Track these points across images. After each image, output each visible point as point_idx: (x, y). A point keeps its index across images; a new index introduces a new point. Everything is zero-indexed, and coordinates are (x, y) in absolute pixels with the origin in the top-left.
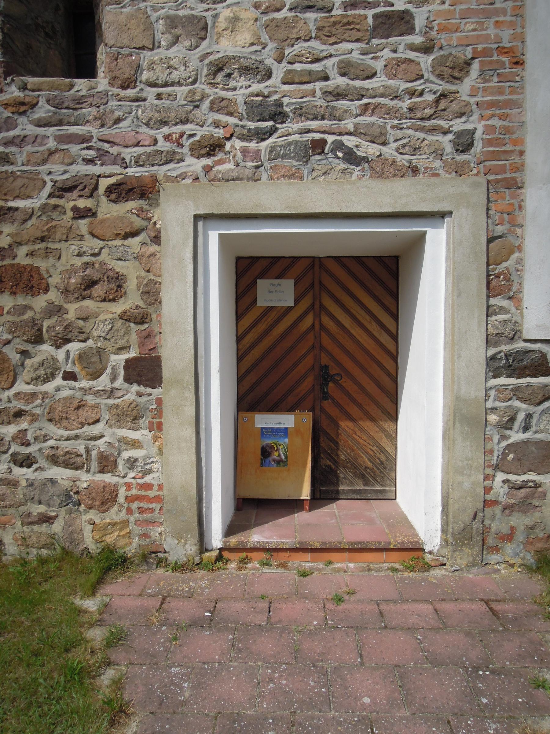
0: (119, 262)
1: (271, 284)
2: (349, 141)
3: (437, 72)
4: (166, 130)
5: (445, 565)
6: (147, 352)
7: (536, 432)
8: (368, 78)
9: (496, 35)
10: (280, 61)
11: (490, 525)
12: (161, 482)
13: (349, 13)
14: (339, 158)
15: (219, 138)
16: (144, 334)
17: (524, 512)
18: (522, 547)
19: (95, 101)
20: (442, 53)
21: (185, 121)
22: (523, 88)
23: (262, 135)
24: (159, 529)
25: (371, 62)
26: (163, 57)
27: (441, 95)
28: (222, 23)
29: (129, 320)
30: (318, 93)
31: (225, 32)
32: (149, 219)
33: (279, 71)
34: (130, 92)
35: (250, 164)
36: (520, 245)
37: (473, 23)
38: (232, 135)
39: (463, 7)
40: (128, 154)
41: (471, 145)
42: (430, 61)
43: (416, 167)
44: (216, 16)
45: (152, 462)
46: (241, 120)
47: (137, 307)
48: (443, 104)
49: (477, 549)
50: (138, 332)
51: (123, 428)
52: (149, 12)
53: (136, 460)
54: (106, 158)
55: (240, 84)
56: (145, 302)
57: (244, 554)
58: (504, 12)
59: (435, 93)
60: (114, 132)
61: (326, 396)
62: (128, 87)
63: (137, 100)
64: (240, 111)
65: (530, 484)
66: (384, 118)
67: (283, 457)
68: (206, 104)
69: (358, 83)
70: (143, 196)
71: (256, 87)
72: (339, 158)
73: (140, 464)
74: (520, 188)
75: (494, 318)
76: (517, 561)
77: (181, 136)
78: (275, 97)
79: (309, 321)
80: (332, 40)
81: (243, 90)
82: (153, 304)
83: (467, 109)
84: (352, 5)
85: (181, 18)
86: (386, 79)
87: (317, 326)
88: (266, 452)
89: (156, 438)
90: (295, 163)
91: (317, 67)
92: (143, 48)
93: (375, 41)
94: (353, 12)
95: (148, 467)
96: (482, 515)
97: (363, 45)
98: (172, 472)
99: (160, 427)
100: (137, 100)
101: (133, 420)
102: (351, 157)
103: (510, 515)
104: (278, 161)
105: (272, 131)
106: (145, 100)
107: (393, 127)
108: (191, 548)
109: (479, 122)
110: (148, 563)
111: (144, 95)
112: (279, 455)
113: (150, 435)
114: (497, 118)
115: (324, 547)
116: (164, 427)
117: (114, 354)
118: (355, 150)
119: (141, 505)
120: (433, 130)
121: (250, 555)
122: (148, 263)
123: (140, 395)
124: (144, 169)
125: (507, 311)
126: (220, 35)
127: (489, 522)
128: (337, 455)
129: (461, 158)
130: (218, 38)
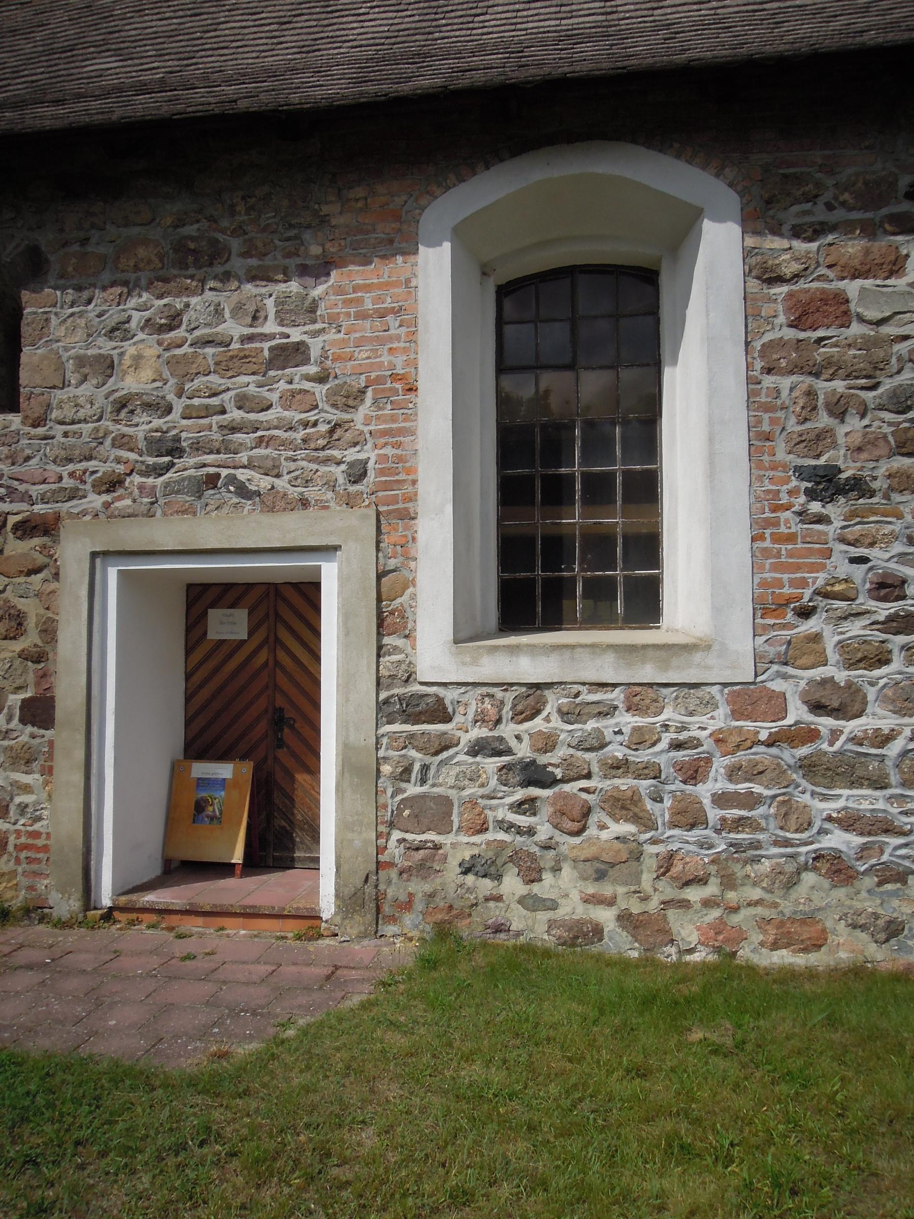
0: (22, 599)
1: (223, 615)
2: (242, 475)
3: (330, 402)
4: (71, 467)
5: (337, 935)
6: (42, 692)
7: (433, 785)
8: (263, 410)
9: (390, 362)
10: (180, 397)
11: (386, 891)
12: (50, 830)
13: (246, 346)
14: (231, 492)
15: (120, 474)
16: (41, 673)
17: (424, 878)
18: (421, 917)
20: (337, 382)
21: (89, 458)
22: (416, 415)
23: (159, 470)
24: (46, 882)
25: (267, 395)
26: (71, 395)
27: (336, 425)
28: (127, 360)
29: (26, 659)
30: (215, 428)
31: (130, 369)
32: (51, 556)
33: (179, 406)
34: (41, 431)
35: (146, 500)
36: (413, 580)
37: (367, 351)
38: (132, 471)
39: (357, 335)
40: (35, 491)
41: (365, 474)
42: (324, 392)
43: (307, 500)
44: (122, 354)
45: (42, 809)
46: (141, 456)
47: (36, 645)
49: (370, 917)
50: (36, 671)
51: (17, 771)
52: (61, 353)
53: (27, 806)
54: (14, 495)
55: (142, 420)
56: (42, 640)
57: (134, 916)
58: (398, 338)
59: (329, 423)
60: (23, 470)
61: (280, 744)
62: (38, 426)
63: (45, 438)
64: (140, 447)
65: (429, 844)
66: (280, 450)
67: (218, 813)
68: (108, 442)
69: (252, 416)
70: (46, 533)
71: (157, 423)
72: (231, 492)
73: (30, 810)
74: (413, 519)
75: (387, 658)
76: (415, 933)
77: (84, 473)
78: (174, 432)
79: (263, 656)
80: (230, 374)
81: (144, 425)
82: (50, 642)
83: (361, 439)
84: (249, 338)
85: (89, 357)
86: (281, 410)
87: (271, 663)
88: (200, 807)
89: (46, 783)
90: (188, 499)
91: (215, 401)
92: (54, 387)
93: (272, 373)
94: (250, 346)
95: (38, 813)
96: (375, 878)
97: (259, 378)
98: (60, 820)
99: (51, 769)
100: (45, 438)
101: (27, 763)
102: (243, 491)
103: (408, 880)
104: (170, 498)
105: (170, 466)
106: (53, 438)
107: (286, 459)
108: (75, 904)
109: (373, 451)
110: (30, 918)
111: (51, 433)
112: (214, 810)
113: (41, 779)
114: (389, 447)
115: (214, 910)
116: (54, 772)
117: (12, 693)
118: (247, 484)
119: (29, 854)
120: (327, 461)
121: (141, 916)
122: (47, 599)
123: (33, 737)
124: (49, 506)
125: (401, 651)
126: (125, 373)
127: (385, 887)
128: (293, 814)
129: (353, 489)
130: (124, 376)
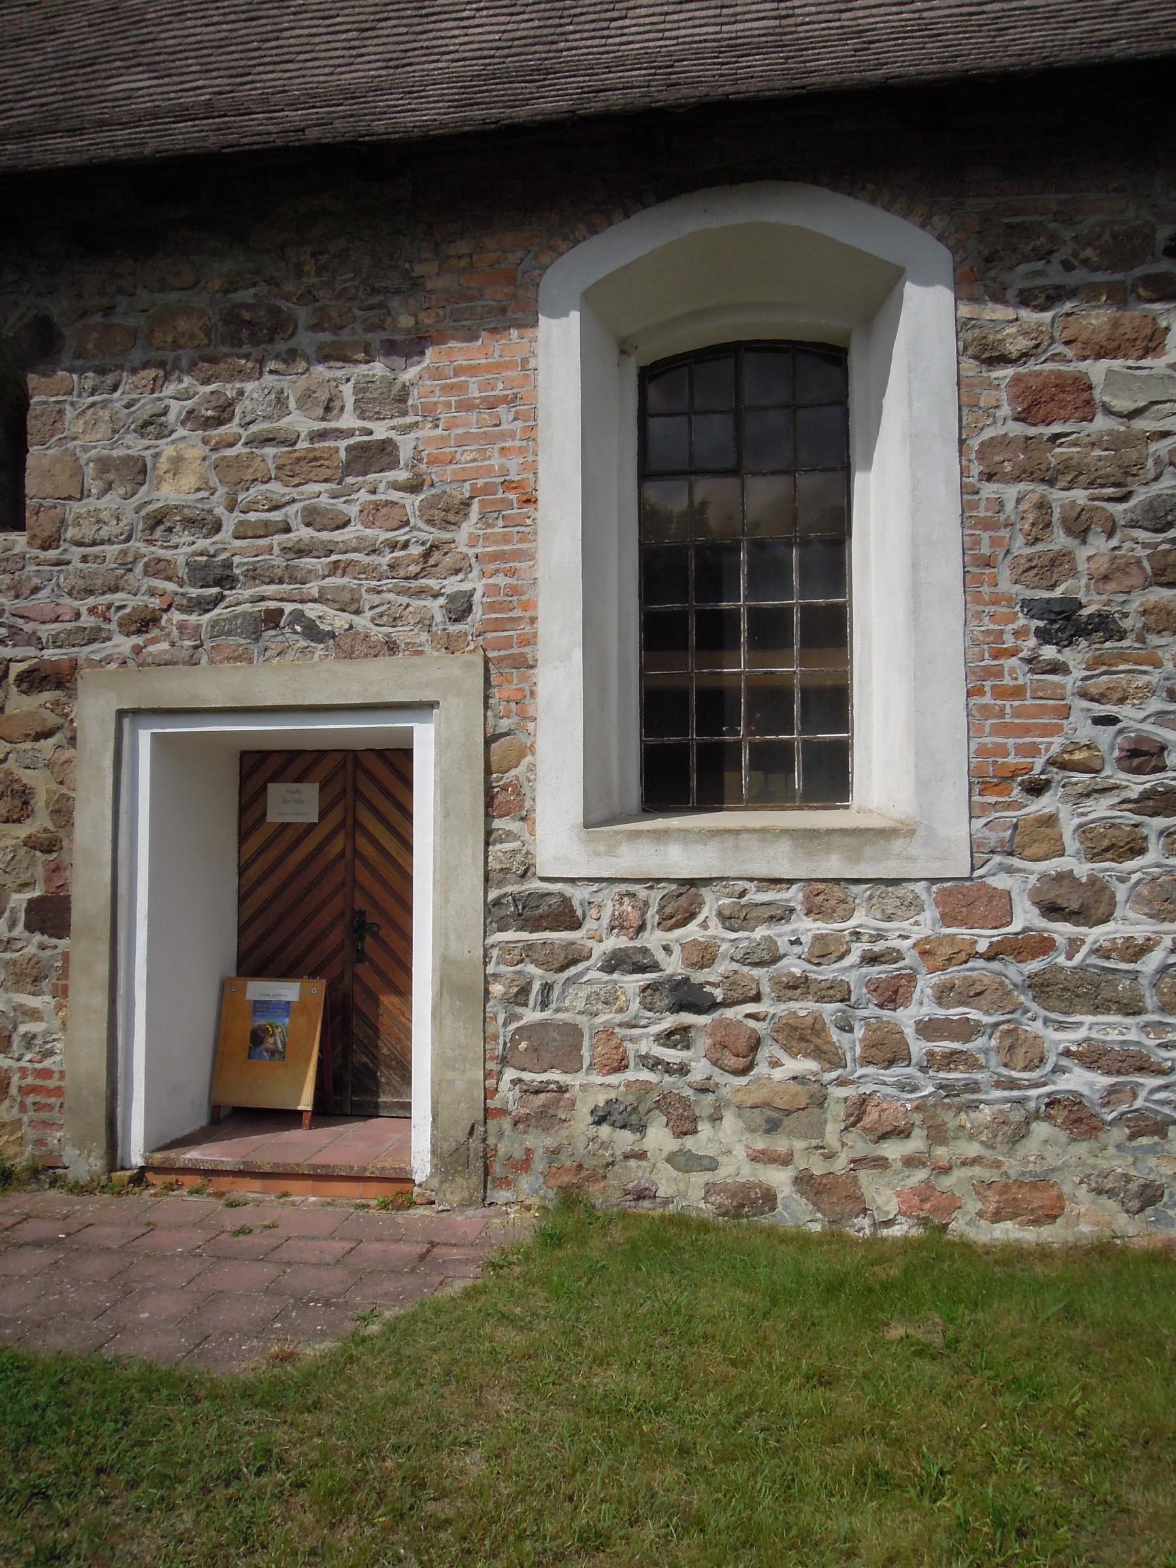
0: (28, 771)
1: (287, 791)
2: (312, 611)
3: (425, 518)
4: (91, 601)
5: (433, 1203)
6: (54, 890)
7: (558, 1010)
8: (338, 528)
9: (502, 466)
10: (231, 510)
11: (496, 1146)
12: (64, 1067)
13: (316, 445)
14: (297, 633)
15: (154, 610)
16: (52, 866)
17: (546, 1130)
18: (541, 1180)
19: (10, 566)
20: (433, 491)
21: (115, 589)
22: (535, 533)
23: (204, 605)
24: (59, 1134)
25: (344, 508)
27: (432, 546)
28: (163, 464)
29: (34, 848)
30: (276, 550)
31: (168, 475)
32: (66, 715)
33: (230, 522)
34: (52, 554)
35: (188, 643)
36: (532, 745)
37: (472, 451)
38: (170, 606)
39: (460, 431)
40: (46, 631)
41: (469, 609)
42: (417, 504)
43: (395, 643)
44: (157, 456)
45: (54, 1040)
46: (181, 586)
47: (46, 830)
48: (435, 557)
49: (476, 1180)
50: (46, 863)
51: (22, 992)
52: (78, 454)
53: (34, 1037)
54: (18, 637)
55: (182, 540)
56: (55, 824)
57: (172, 1178)
58: (512, 435)
59: (423, 544)
60: (30, 604)
62: (49, 547)
63: (58, 563)
64: (180, 575)
65: (552, 1086)
66: (360, 579)
67: (280, 1046)
68: (139, 568)
69: (325, 535)
70: (59, 685)
71: (202, 544)
72: (297, 633)
73: (38, 1041)
74: (532, 667)
75: (498, 847)
76: (534, 1201)
77: (109, 608)
78: (223, 556)
79: (338, 844)
80: (296, 481)
81: (186, 547)
82: (64, 826)
83: (465, 564)
84: (320, 435)
85: (115, 460)
86: (362, 528)
87: (349, 853)
88: (257, 1037)
89: (60, 1007)
90: (242, 641)
91: (276, 516)
92: (69, 498)
93: (350, 480)
94: (321, 445)
95: (49, 1046)
96: (482, 1129)
97: (333, 486)
98: (77, 1054)
99: (65, 989)
100: (58, 563)
101: (34, 981)
102: (313, 632)
103: (525, 1132)
104: (218, 641)
105: (218, 600)
106: (68, 563)
107: (368, 591)
108: (96, 1163)
109: (480, 580)
110: (38, 1180)
111: (66, 557)
112: (275, 1042)
113: (53, 1002)
114: (501, 575)
115: (276, 1170)
116: (70, 992)
117: (15, 891)
118: (318, 623)
119: (38, 1099)
120: (420, 593)
121: (181, 1178)
122: (61, 771)
123: (43, 947)
124: (63, 651)
125: (516, 838)
126: (161, 480)
127: (495, 1141)
128: (377, 1047)
129: (454, 628)
130: (159, 483)
